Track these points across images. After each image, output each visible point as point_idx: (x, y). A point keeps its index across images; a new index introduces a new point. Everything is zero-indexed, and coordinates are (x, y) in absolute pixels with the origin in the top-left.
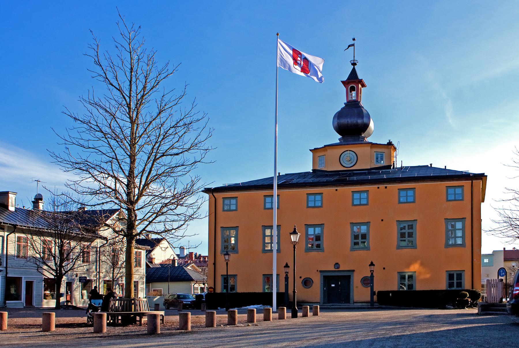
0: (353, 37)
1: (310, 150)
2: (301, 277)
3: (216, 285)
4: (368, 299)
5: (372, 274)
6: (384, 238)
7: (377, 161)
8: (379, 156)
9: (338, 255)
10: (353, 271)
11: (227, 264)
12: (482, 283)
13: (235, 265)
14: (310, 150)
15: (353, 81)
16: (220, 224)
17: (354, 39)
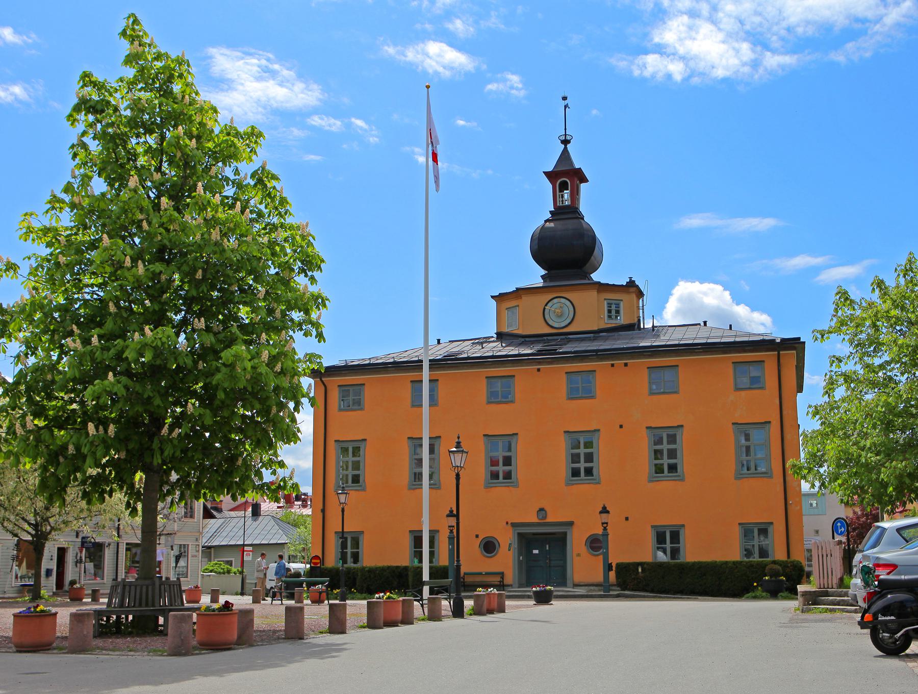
0: (563, 95)
1: (492, 297)
2: (477, 536)
3: (326, 553)
4: (600, 578)
5: (605, 529)
6: (624, 461)
7: (610, 317)
8: (613, 307)
9: (542, 490)
10: (571, 524)
11: (343, 510)
12: (806, 547)
13: (358, 512)
14: (492, 297)
15: (566, 176)
16: (333, 436)
17: (565, 98)
